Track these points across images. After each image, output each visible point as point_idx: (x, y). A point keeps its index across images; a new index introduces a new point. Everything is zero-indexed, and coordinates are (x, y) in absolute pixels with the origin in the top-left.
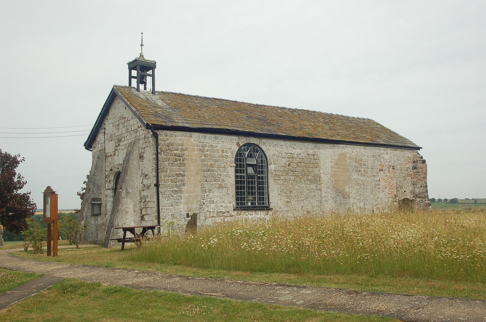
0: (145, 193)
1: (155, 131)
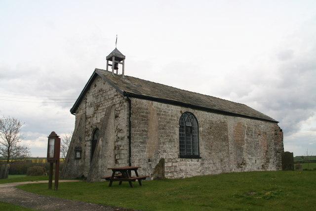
0: (119, 143)
1: (129, 98)
